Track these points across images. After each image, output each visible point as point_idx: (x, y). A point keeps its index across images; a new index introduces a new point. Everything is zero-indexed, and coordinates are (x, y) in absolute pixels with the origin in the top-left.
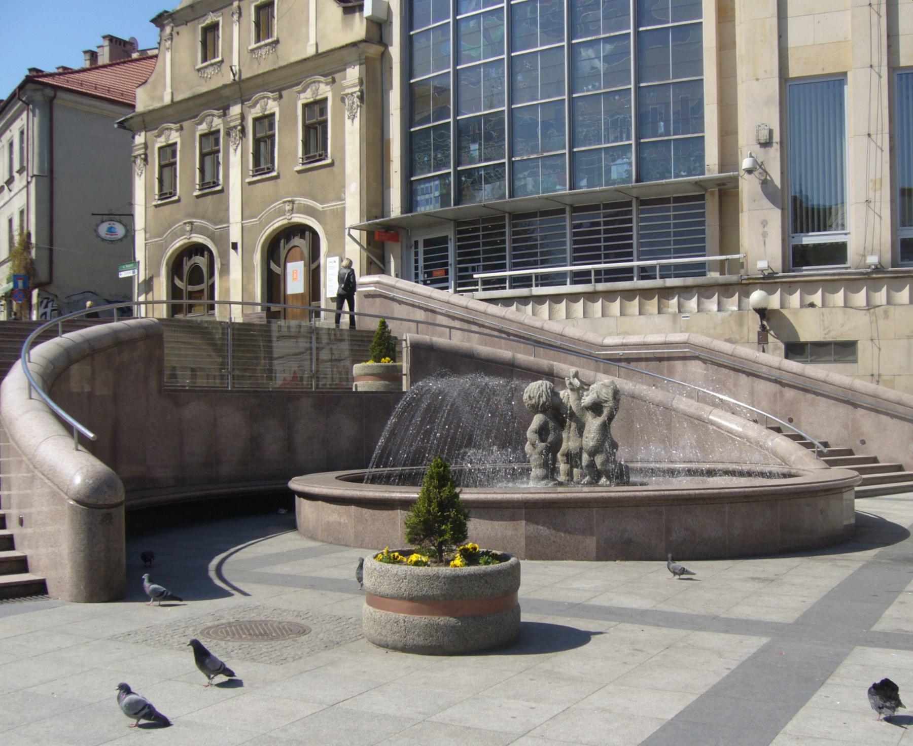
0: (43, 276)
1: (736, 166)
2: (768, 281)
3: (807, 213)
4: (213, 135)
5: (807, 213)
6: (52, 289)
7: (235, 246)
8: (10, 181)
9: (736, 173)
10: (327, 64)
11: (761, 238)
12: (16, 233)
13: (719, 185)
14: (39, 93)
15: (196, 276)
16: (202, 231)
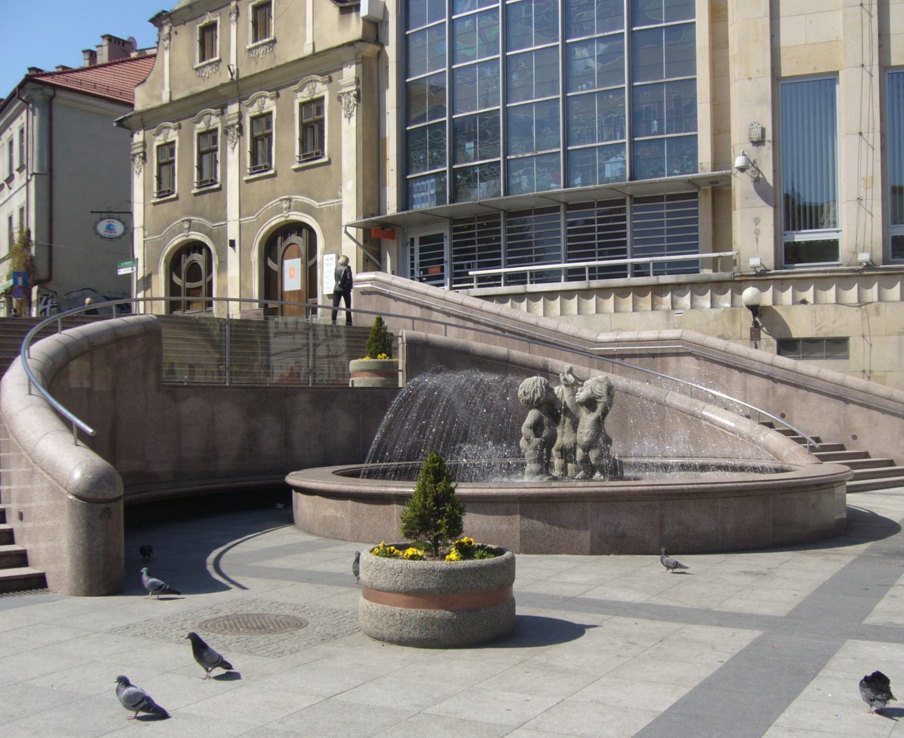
0: (43, 273)
1: (728, 164)
2: (760, 278)
3: (799, 210)
4: (211, 133)
5: (799, 210)
6: (52, 286)
7: (232, 243)
8: (10, 179)
9: (729, 171)
10: (323, 63)
11: (753, 235)
12: (16, 231)
13: (712, 183)
14: (39, 92)
15: (194, 273)
16: (200, 229)
